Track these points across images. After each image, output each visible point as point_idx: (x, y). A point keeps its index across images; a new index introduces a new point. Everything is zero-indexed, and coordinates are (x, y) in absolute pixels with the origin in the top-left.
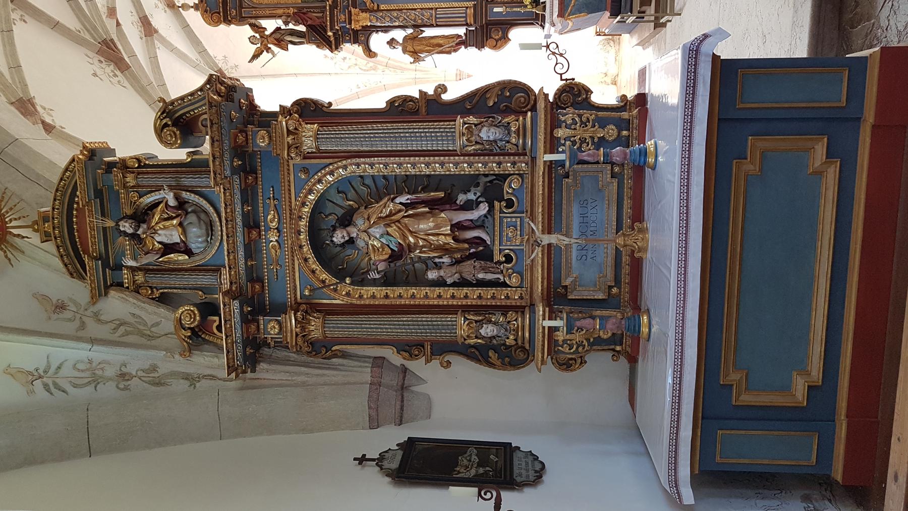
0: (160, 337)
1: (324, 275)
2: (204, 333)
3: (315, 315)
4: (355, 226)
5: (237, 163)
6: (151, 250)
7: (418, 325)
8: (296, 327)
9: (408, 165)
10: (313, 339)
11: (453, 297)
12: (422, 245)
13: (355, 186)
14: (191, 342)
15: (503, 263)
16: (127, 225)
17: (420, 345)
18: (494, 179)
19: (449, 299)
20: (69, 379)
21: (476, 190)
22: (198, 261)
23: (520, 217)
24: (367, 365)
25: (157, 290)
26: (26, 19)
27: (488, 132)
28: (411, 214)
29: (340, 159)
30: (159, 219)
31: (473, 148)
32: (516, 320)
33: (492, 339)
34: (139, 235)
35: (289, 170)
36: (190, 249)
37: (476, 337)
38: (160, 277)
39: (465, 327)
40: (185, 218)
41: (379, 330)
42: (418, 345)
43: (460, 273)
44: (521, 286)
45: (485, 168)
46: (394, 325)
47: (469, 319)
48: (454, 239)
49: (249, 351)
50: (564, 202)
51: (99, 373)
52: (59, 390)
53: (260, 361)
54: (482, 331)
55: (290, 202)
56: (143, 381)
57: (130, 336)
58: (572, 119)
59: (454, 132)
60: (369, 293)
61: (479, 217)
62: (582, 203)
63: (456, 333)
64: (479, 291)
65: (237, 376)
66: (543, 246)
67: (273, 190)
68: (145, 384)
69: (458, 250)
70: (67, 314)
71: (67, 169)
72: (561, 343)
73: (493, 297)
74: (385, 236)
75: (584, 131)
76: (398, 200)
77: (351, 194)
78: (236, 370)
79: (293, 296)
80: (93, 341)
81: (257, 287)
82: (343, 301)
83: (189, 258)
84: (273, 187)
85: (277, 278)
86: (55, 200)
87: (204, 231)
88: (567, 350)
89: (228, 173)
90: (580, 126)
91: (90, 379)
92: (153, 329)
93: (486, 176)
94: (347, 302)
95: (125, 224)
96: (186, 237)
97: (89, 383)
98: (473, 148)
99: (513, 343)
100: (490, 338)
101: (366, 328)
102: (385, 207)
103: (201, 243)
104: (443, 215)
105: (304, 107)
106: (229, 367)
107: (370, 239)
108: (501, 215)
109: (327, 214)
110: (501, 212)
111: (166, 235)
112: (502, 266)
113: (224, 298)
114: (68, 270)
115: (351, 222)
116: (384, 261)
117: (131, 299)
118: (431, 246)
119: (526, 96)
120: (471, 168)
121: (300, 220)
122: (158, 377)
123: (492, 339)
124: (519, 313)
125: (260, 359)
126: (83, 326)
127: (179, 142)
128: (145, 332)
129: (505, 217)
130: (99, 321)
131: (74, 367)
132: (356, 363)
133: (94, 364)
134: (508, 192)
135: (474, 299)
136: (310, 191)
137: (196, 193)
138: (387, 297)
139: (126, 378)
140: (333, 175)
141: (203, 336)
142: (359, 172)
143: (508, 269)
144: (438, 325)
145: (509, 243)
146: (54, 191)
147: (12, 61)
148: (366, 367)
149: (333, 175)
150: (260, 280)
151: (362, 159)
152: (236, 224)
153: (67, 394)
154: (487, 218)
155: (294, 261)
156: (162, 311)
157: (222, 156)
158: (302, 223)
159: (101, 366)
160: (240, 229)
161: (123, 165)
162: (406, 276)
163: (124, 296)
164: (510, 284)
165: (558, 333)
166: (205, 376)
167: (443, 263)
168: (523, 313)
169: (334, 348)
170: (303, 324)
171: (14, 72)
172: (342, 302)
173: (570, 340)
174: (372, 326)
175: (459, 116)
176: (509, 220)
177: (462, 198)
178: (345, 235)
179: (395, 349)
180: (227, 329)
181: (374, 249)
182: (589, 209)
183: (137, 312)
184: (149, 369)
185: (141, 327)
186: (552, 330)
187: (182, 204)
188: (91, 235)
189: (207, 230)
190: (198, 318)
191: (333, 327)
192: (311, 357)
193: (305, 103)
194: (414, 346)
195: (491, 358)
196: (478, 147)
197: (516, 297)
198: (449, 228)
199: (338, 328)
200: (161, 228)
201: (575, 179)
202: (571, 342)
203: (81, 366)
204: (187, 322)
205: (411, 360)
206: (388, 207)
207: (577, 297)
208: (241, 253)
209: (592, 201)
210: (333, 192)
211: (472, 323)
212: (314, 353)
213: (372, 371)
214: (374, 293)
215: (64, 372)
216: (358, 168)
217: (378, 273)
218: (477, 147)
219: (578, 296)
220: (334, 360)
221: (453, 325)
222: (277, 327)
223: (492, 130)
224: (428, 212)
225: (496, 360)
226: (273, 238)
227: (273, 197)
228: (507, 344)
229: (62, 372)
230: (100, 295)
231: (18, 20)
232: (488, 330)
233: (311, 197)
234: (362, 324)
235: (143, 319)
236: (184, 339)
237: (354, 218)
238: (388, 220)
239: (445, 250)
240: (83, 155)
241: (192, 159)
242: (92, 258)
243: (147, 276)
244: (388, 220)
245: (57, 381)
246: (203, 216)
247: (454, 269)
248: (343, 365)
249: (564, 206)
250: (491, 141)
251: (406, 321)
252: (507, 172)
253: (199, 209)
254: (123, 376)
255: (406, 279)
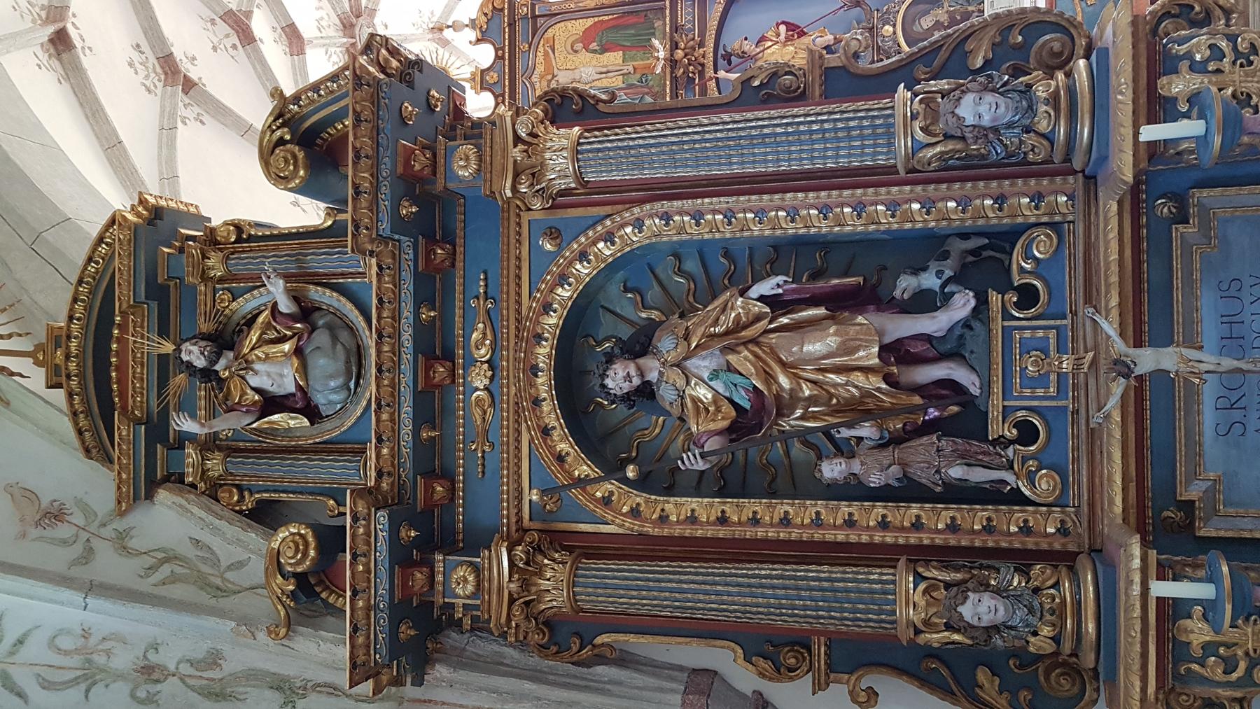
0: (239, 592)
1: (585, 468)
2: (327, 588)
3: (556, 555)
4: (657, 354)
5: (407, 209)
6: (239, 403)
7: (798, 588)
8: (510, 581)
9: (780, 213)
10: (549, 613)
11: (884, 525)
12: (810, 397)
13: (662, 276)
14: (292, 604)
15: (1012, 442)
16: (195, 349)
17: (801, 643)
18: (983, 248)
19: (874, 528)
20: (37, 669)
21: (939, 266)
22: (330, 431)
23: (1056, 328)
24: (674, 685)
25: (251, 494)
26: (204, 120)
27: (977, 104)
28: (787, 324)
29: (627, 206)
30: (258, 340)
31: (938, 149)
32: (1056, 585)
33: (992, 633)
34: (217, 372)
35: (519, 234)
36: (316, 407)
37: (948, 627)
38: (253, 463)
39: (918, 597)
40: (309, 337)
41: (701, 597)
42: (793, 644)
43: (903, 464)
44: (1061, 502)
45: (964, 211)
46: (738, 585)
47: (926, 578)
48: (887, 378)
49: (406, 631)
50: (1177, 283)
51: (100, 659)
52: (12, 691)
53: (438, 661)
54: (967, 611)
55: (519, 303)
56: (188, 686)
57: (178, 585)
58: (1210, 47)
59: (892, 116)
60: (683, 512)
61: (951, 330)
62: (1225, 287)
63: (894, 613)
64: (951, 513)
65: (377, 690)
66: (1140, 378)
67: (486, 279)
68: (191, 694)
69: (892, 412)
70: (63, 531)
71: (100, 240)
72: (1198, 653)
73: (988, 529)
74: (721, 374)
75: (1247, 75)
76: (755, 291)
77: (654, 294)
78: (376, 675)
79: (513, 511)
80: (93, 588)
81: (439, 488)
82: (622, 526)
83: (312, 424)
84: (485, 273)
85: (483, 472)
86: (75, 300)
87: (341, 365)
88: (1218, 674)
89: (385, 227)
90: (1234, 63)
91: (79, 673)
92: (229, 575)
93: (964, 236)
94: (632, 530)
95: (192, 348)
96: (307, 380)
97: (75, 682)
98: (938, 149)
99: (1049, 648)
100: (986, 628)
101: (671, 590)
102: (724, 310)
103: (335, 390)
104: (860, 319)
105: (560, 105)
106: (354, 666)
107: (688, 383)
108: (1006, 324)
109: (601, 337)
110: (1007, 316)
111: (269, 375)
112: (1010, 452)
113: (354, 503)
114: (83, 442)
115: (648, 347)
116: (719, 433)
117: (195, 510)
118: (831, 399)
119: (1066, 38)
120: (928, 213)
121: (539, 344)
122: (221, 679)
123: (992, 633)
124: (1064, 571)
125: (436, 655)
126: (88, 555)
127: (302, 173)
128: (212, 579)
129: (1016, 328)
130: (125, 550)
131: (52, 643)
132: (651, 681)
133: (93, 641)
134: (1021, 270)
135: (938, 531)
136: (562, 279)
137: (334, 287)
138: (723, 520)
139: (155, 676)
140: (613, 244)
141: (324, 595)
142: (670, 235)
143: (1024, 460)
144: (847, 590)
145: (1027, 392)
146: (74, 279)
147: (166, 169)
148: (673, 691)
149: (613, 244)
150: (448, 477)
151: (675, 203)
152: (401, 345)
153: (26, 702)
154: (971, 328)
155: (520, 433)
156: (253, 537)
157: (376, 188)
158: (541, 351)
159: (107, 645)
160: (407, 356)
161: (212, 240)
162: (769, 479)
163: (184, 502)
164: (1033, 497)
165: (1188, 622)
166: (319, 685)
167: (860, 439)
168: (1071, 569)
169: (599, 640)
170: (525, 573)
171: (166, 185)
172: (620, 531)
173: (1228, 646)
174: (685, 586)
175: (902, 85)
176: (1027, 334)
177: (906, 285)
178: (633, 372)
179: (740, 651)
180: (357, 576)
181: (697, 408)
182: (1247, 303)
183: (205, 537)
184: (203, 660)
185: (205, 569)
186: (1171, 610)
187: (307, 312)
188: (134, 373)
189: (348, 362)
190: (312, 553)
191: (596, 586)
192: (546, 657)
193: (561, 96)
194: (786, 644)
195: (981, 687)
196: (951, 146)
197: (1051, 530)
198: (876, 349)
199: (606, 587)
200: (259, 358)
201: (1205, 226)
202: (1230, 652)
203: (66, 643)
204: (289, 561)
205: (779, 681)
206: (732, 308)
207: (1222, 534)
208: (407, 409)
209: (1253, 281)
210: (614, 288)
211: (936, 588)
212: (554, 649)
213: (684, 703)
214: (693, 511)
215: (30, 652)
216: (667, 224)
217: (702, 457)
218: (950, 147)
219: (1226, 530)
220: (600, 669)
221: (886, 593)
222: (471, 578)
223: (989, 98)
224: (825, 318)
225: (994, 694)
226: (480, 380)
227: (485, 293)
228: (1032, 649)
229: (27, 653)
230: (136, 498)
231: (192, 119)
232: (983, 609)
233: (564, 293)
234: (659, 581)
235: (213, 553)
236: (278, 597)
237: (654, 341)
238: (733, 338)
239: (858, 409)
240: (138, 215)
241: (334, 222)
242: (128, 419)
243: (230, 462)
244: (733, 338)
245: (12, 670)
246: (344, 336)
247: (887, 455)
248: (620, 683)
249: (1178, 295)
250: (985, 129)
251: (766, 577)
252: (1020, 220)
253: (340, 321)
254: (149, 672)
255: (770, 484)
